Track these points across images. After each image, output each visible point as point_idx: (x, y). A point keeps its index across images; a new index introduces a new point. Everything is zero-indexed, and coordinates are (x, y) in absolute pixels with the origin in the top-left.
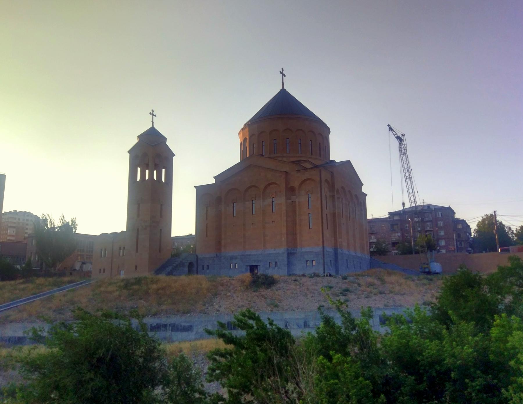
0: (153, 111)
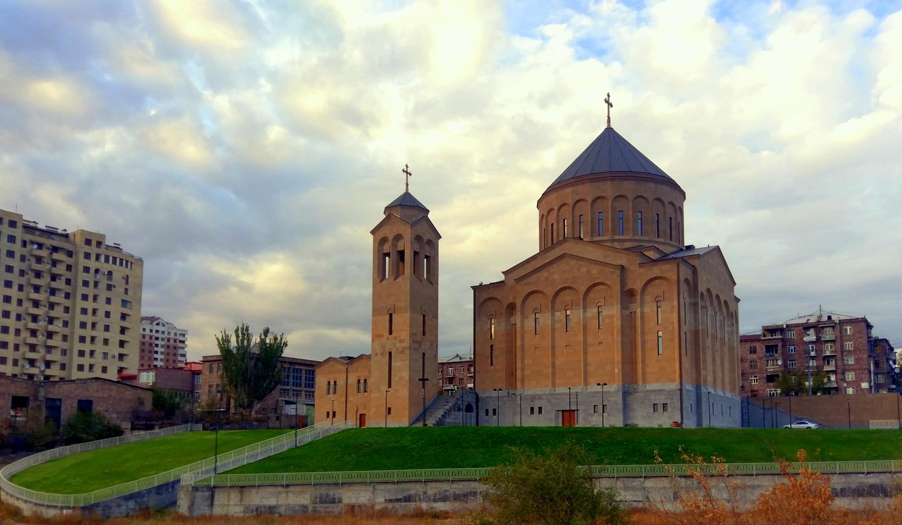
0: (407, 166)
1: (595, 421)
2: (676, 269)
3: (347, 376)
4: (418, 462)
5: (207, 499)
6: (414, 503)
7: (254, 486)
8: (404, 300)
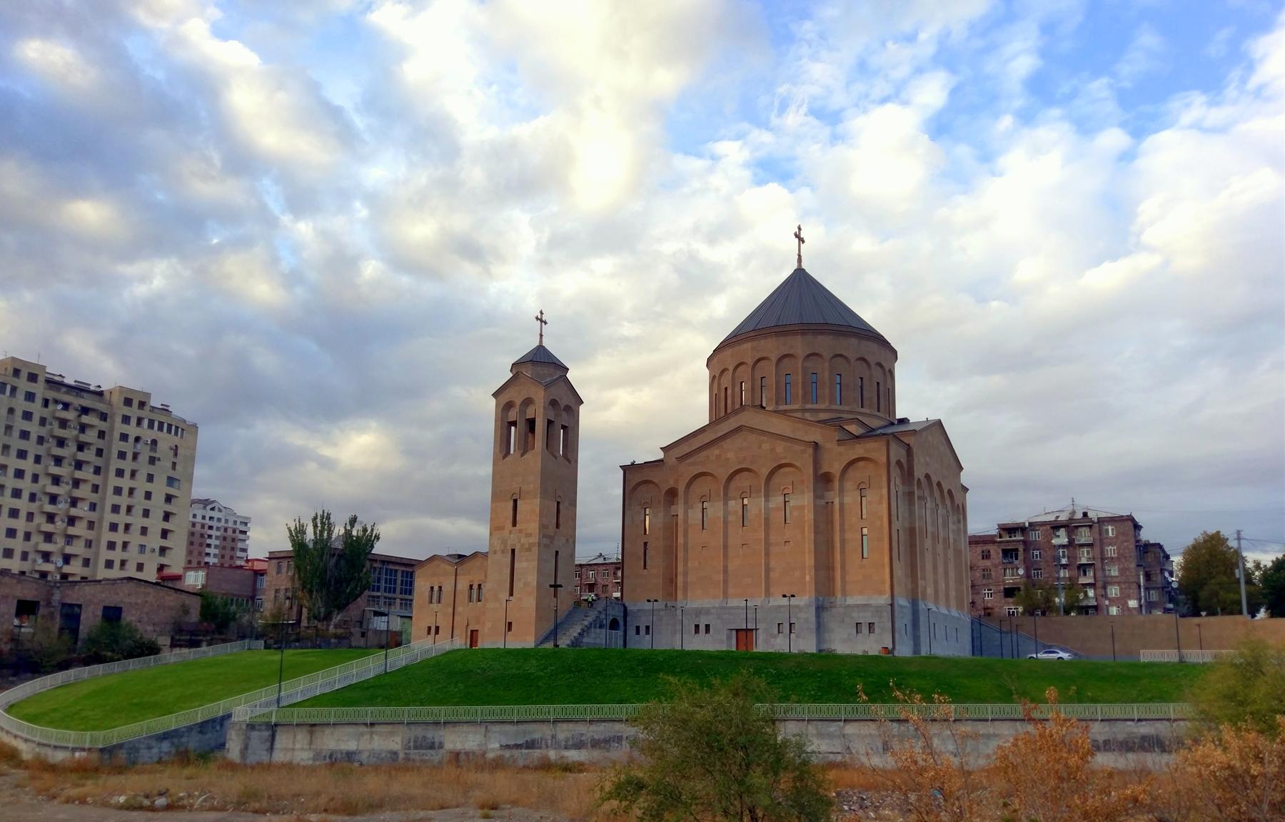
0: (541, 313)
1: (779, 644)
5: (266, 741)
6: (539, 751)
7: (328, 724)
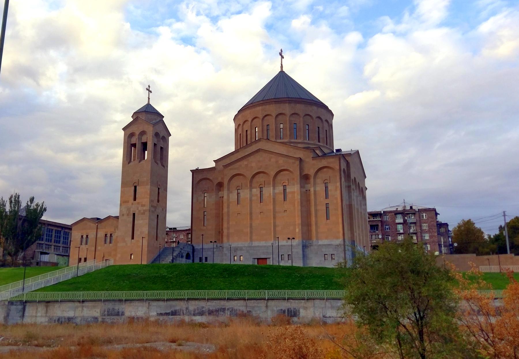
0: (149, 86)
2: (338, 162)
3: (97, 231)
4: (177, 287)
6: (179, 316)
7: (57, 301)
8: (146, 177)
